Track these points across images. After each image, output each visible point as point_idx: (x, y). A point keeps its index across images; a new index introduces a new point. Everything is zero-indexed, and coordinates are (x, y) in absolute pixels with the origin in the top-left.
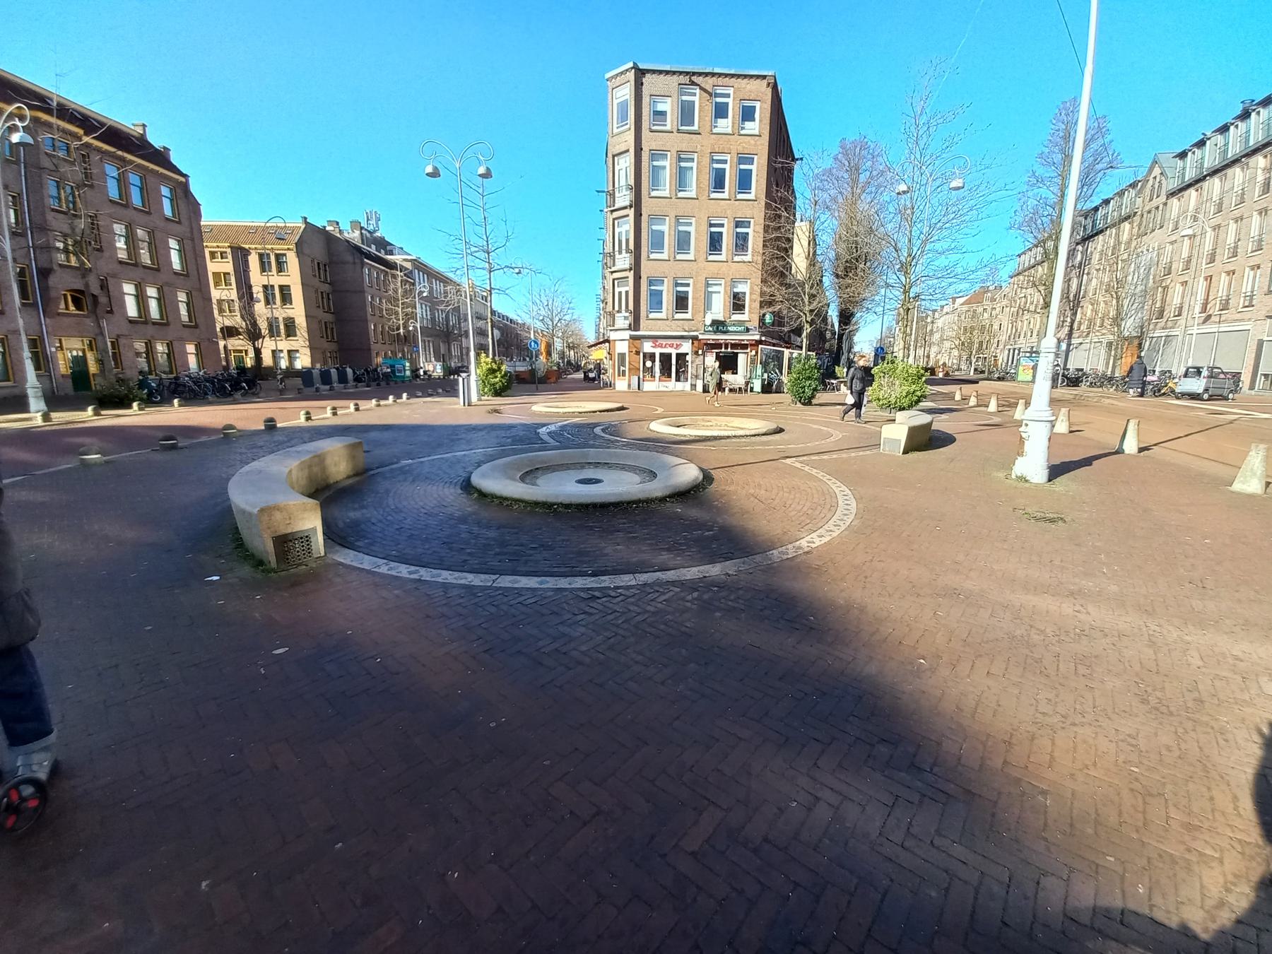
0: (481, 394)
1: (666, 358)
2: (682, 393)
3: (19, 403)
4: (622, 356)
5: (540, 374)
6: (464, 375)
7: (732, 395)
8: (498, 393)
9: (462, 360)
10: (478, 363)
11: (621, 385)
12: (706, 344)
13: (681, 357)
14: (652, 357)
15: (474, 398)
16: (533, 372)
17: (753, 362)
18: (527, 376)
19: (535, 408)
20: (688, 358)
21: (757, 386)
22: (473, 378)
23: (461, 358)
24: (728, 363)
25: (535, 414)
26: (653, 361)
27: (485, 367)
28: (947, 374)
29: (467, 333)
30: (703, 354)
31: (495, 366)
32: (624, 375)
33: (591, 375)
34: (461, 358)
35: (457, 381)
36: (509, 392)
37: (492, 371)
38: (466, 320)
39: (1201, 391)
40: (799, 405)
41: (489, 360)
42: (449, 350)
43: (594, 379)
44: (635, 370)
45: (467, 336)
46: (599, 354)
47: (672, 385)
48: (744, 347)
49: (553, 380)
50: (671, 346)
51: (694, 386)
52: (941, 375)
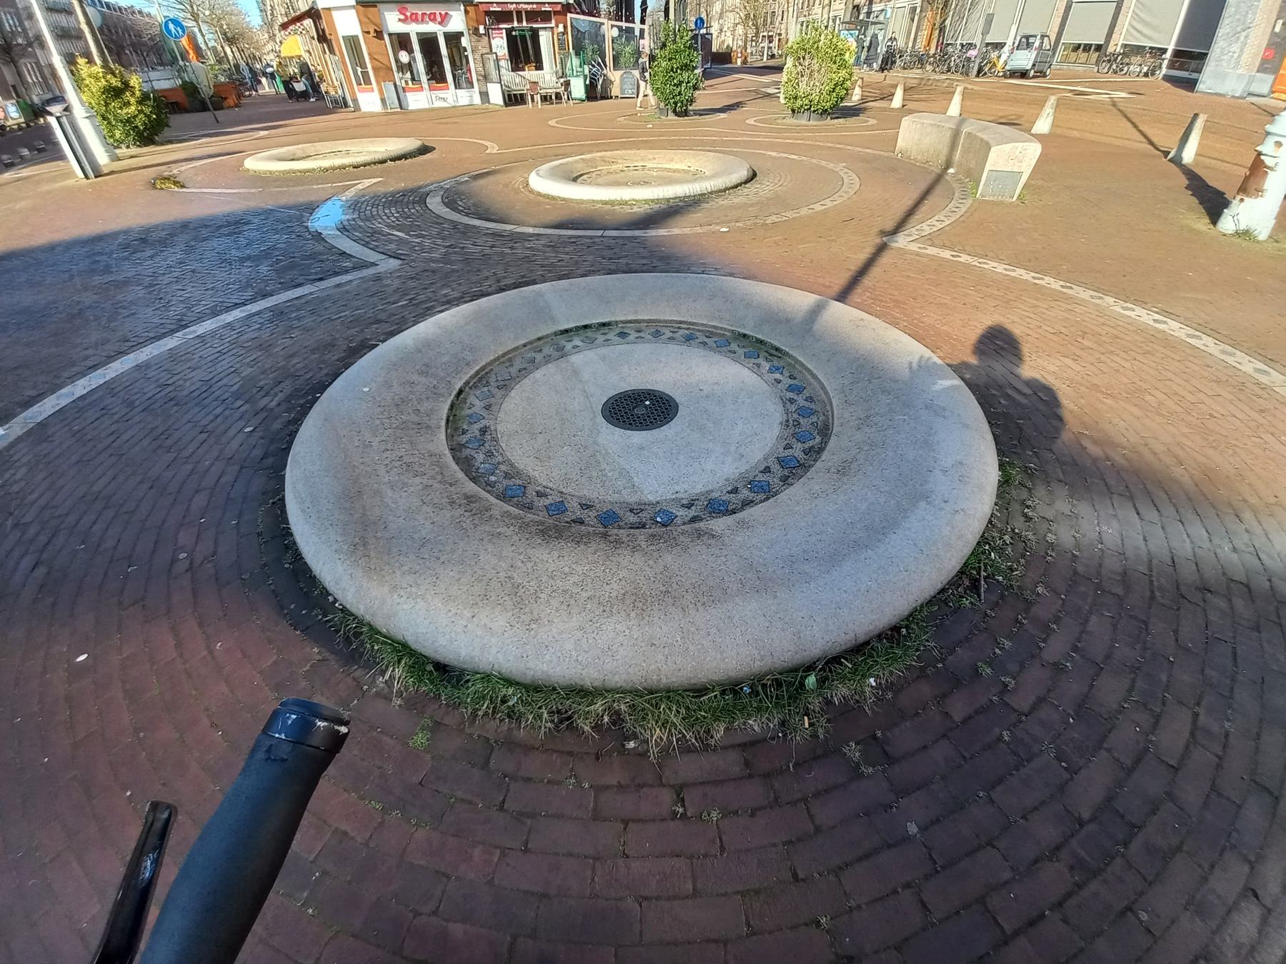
0: (112, 145)
1: (429, 44)
2: (469, 111)
3: (29, 142)
4: (352, 42)
5: (206, 90)
6: (56, 109)
7: (548, 107)
8: (148, 135)
9: (49, 89)
10: (79, 83)
11: (369, 101)
12: (488, 13)
13: (453, 39)
14: (402, 42)
15: (102, 157)
16: (190, 89)
17: (562, 45)
18: (181, 98)
19: (251, 164)
20: (465, 42)
21: (578, 88)
22: (79, 112)
23: (45, 84)
24: (523, 52)
25: (262, 180)
26: (410, 51)
27: (96, 87)
28: (745, 62)
29: (39, 39)
30: (487, 34)
31: (115, 82)
32: (368, 82)
33: (299, 87)
34: (45, 84)
35: (48, 127)
36: (167, 133)
37: (115, 93)
38: (31, 16)
39: (1029, 67)
40: (672, 116)
41: (97, 69)
42: (20, 74)
43: (304, 95)
44: (384, 72)
45: (42, 45)
46: (297, 45)
47: (453, 96)
48: (546, 17)
49: (231, 102)
50: (432, 18)
51: (485, 95)
52: (739, 61)
